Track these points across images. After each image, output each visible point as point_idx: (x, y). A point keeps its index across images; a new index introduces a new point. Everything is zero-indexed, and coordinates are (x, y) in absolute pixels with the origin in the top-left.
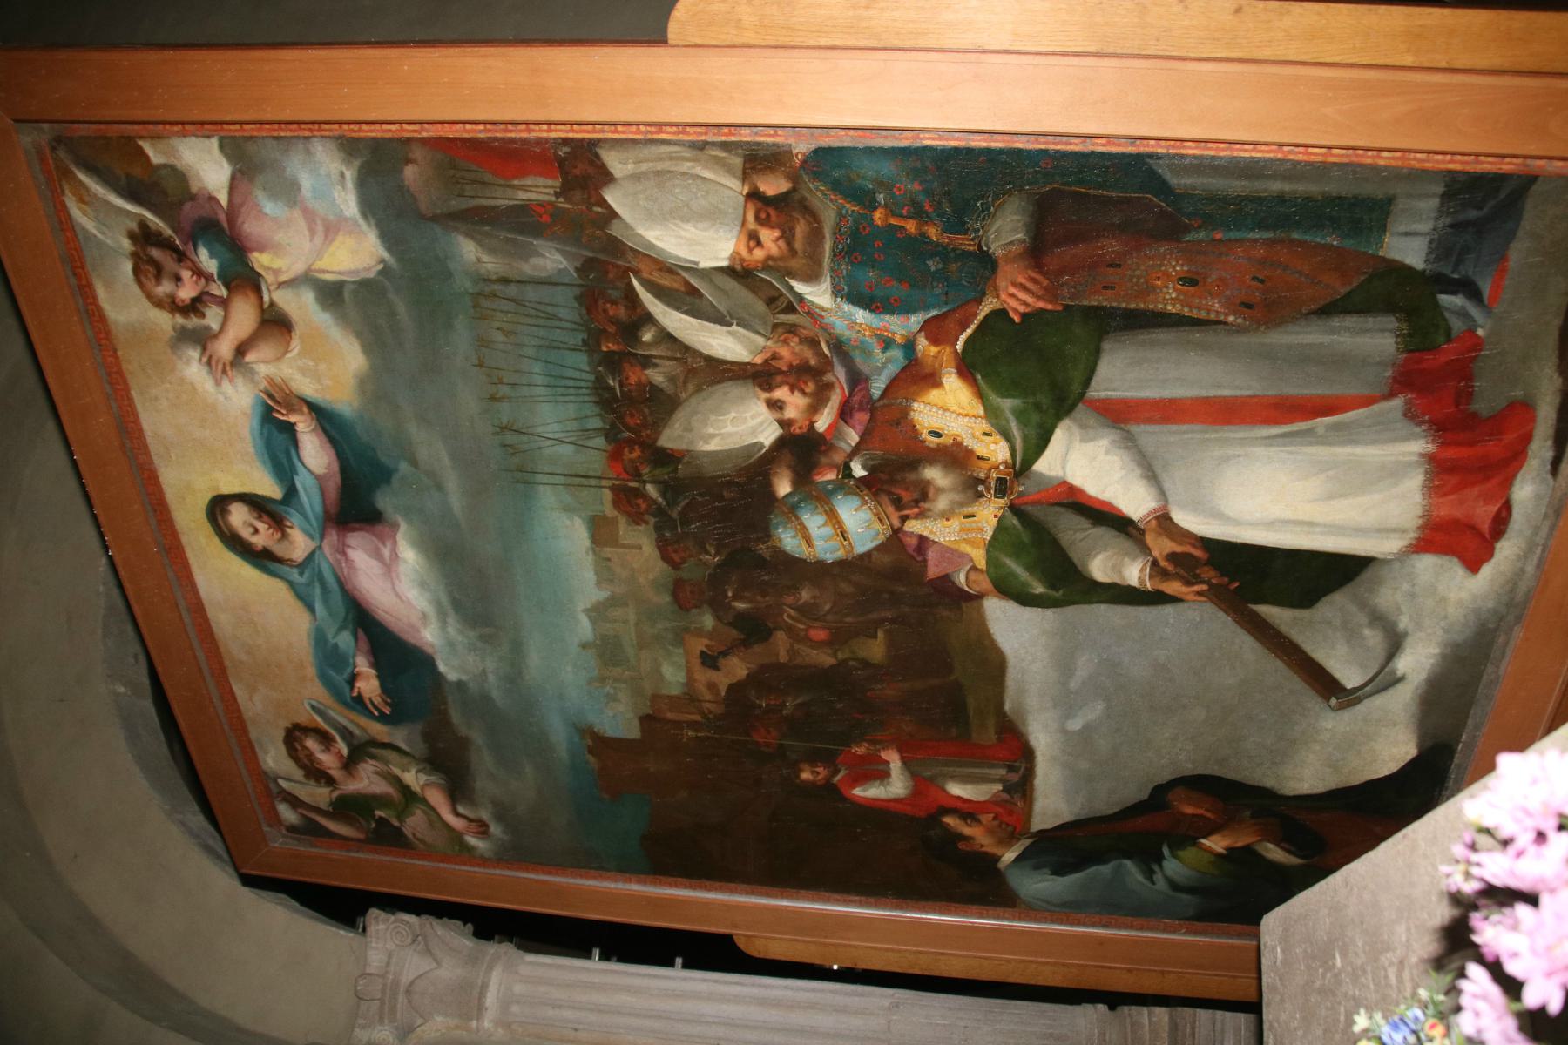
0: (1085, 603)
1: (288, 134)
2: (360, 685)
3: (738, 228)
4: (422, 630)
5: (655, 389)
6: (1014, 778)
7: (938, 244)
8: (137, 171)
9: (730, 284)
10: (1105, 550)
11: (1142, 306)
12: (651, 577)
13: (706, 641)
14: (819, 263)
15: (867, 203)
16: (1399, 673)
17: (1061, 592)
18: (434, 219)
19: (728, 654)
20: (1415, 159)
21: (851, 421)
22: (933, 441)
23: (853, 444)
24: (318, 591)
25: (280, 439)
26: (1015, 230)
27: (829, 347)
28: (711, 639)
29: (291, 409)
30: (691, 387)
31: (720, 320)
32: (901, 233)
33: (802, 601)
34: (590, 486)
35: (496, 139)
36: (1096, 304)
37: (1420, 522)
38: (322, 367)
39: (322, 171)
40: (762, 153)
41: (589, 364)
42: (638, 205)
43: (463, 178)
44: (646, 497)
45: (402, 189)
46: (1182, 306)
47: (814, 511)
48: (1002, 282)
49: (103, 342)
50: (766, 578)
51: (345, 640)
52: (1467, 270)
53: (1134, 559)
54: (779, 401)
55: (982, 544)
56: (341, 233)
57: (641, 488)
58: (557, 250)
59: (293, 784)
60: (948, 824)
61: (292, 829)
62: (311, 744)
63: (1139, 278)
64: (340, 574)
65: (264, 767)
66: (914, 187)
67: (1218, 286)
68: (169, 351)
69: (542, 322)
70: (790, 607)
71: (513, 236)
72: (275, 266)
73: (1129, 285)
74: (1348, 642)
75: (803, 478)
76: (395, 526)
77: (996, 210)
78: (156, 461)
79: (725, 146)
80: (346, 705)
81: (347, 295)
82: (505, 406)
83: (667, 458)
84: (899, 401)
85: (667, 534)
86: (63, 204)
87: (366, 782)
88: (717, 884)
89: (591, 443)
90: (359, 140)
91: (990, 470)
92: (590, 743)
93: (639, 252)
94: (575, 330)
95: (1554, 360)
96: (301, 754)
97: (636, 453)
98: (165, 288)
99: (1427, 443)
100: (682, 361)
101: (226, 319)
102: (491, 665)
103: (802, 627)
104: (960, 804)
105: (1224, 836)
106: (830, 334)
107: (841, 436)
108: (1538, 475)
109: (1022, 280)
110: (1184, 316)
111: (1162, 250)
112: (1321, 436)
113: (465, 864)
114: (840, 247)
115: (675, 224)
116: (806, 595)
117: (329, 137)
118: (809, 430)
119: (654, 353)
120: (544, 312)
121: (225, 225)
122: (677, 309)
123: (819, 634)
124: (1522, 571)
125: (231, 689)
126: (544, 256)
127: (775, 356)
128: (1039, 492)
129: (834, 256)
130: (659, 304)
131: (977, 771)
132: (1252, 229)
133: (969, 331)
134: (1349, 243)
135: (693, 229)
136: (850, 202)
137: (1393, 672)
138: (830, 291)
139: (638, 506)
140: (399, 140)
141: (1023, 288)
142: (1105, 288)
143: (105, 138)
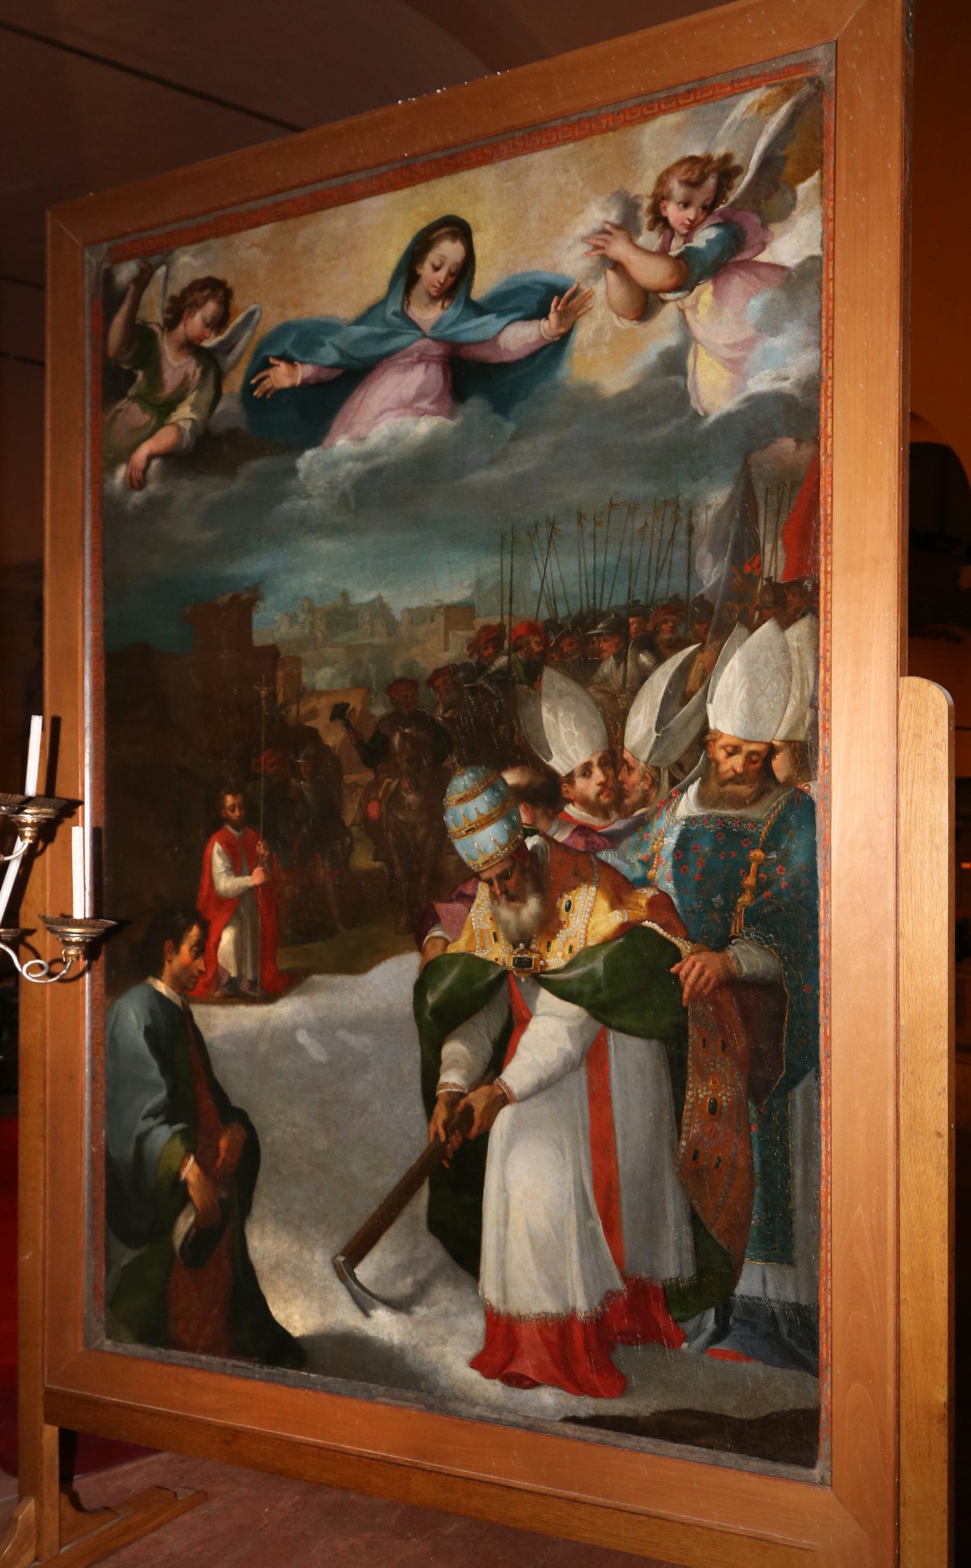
0: (421, 1038)
1: (824, 326)
2: (283, 367)
3: (742, 737)
4: (347, 436)
5: (596, 665)
6: (244, 987)
7: (735, 903)
8: (789, 168)
9: (694, 730)
10: (471, 1053)
11: (690, 1071)
12: (418, 660)
13: (359, 708)
14: (715, 805)
15: (768, 844)
16: (373, 1313)
17: (429, 1018)
18: (746, 466)
19: (348, 729)
20: (827, 1280)
21: (576, 834)
22: (562, 903)
23: (555, 837)
24: (379, 330)
25: (532, 303)
26: (750, 966)
27: (641, 815)
28: (361, 712)
29: (562, 315)
30: (599, 696)
31: (661, 722)
32: (743, 873)
33: (404, 794)
34: (502, 606)
35: (819, 524)
36: (690, 1033)
37: (514, 1314)
38: (604, 350)
39: (789, 359)
40: (809, 756)
41: (616, 606)
42: (761, 651)
43: (783, 493)
44: (495, 655)
45: (773, 436)
46: (692, 1103)
47: (490, 804)
48: (706, 956)
49: (622, 117)
50: (425, 763)
51: (329, 354)
52: (737, 1331)
53: (465, 1078)
54: (591, 773)
55: (470, 949)
56: (732, 375)
57: (503, 652)
58: (720, 579)
59: (162, 281)
60: (190, 930)
61: (109, 276)
62: (211, 307)
63: (714, 1067)
64: (398, 356)
65: (178, 252)
66: (783, 883)
67: (711, 1131)
68: (615, 189)
69: (654, 564)
70: (398, 784)
71: (731, 539)
72: (700, 307)
73: (708, 1059)
74: (399, 1265)
75: (521, 794)
76: (451, 415)
77: (765, 949)
78: (503, 164)
79: (814, 725)
80: (259, 351)
81: (673, 378)
82: (574, 528)
83: (533, 675)
84: (596, 875)
85: (461, 675)
86: (758, 86)
87: (176, 364)
88: (102, 716)
89: (543, 606)
90: (819, 396)
91: (538, 953)
92: (244, 597)
93: (719, 652)
94: (647, 593)
95: (665, 1407)
96: (198, 295)
97: (536, 648)
98: (677, 190)
99: (585, 1313)
100: (623, 689)
101: (649, 253)
102: (317, 503)
103: (380, 795)
104: (213, 940)
105: (199, 1178)
106: (653, 815)
107: (562, 827)
108: (563, 1407)
109: (707, 972)
110: (684, 1105)
111: (739, 1084)
112: (585, 1224)
113: (92, 462)
114: (730, 822)
115: (745, 684)
116: (411, 798)
117: (821, 367)
118: (565, 799)
119: (629, 664)
120: (663, 566)
121: (738, 258)
122: (670, 685)
123: (374, 810)
124: (475, 1405)
125: (265, 223)
126: (714, 566)
127: (631, 769)
128: (521, 995)
129: (722, 818)
130: (673, 669)
131: (249, 953)
132: (761, 1155)
133: (661, 931)
134: (753, 1233)
135: (741, 698)
136: (768, 829)
137: (373, 1307)
138: (691, 815)
139: (486, 648)
140: (818, 434)
141: (701, 974)
142: (704, 1040)
143: (822, 137)
